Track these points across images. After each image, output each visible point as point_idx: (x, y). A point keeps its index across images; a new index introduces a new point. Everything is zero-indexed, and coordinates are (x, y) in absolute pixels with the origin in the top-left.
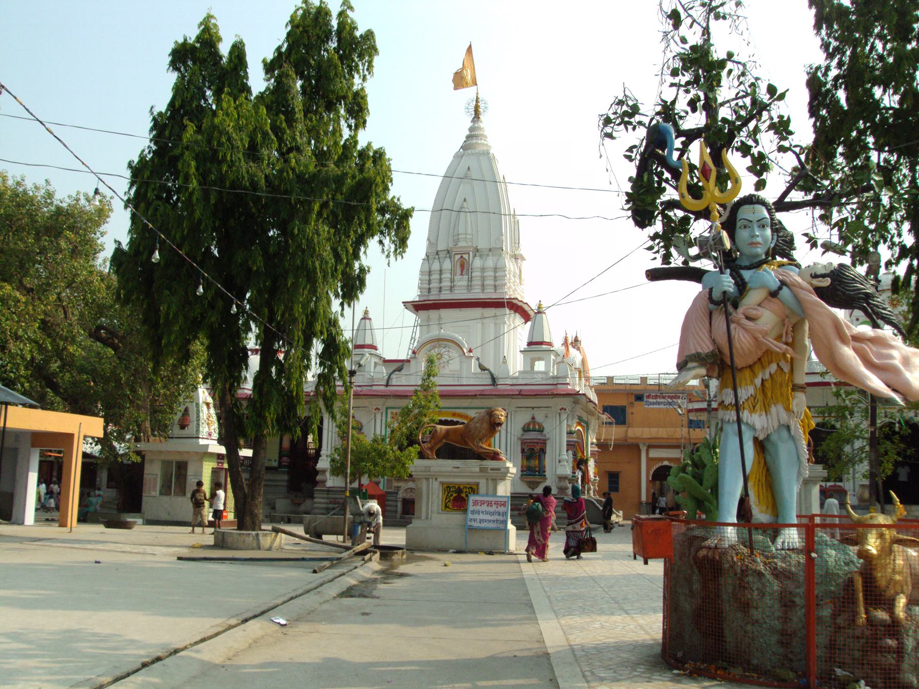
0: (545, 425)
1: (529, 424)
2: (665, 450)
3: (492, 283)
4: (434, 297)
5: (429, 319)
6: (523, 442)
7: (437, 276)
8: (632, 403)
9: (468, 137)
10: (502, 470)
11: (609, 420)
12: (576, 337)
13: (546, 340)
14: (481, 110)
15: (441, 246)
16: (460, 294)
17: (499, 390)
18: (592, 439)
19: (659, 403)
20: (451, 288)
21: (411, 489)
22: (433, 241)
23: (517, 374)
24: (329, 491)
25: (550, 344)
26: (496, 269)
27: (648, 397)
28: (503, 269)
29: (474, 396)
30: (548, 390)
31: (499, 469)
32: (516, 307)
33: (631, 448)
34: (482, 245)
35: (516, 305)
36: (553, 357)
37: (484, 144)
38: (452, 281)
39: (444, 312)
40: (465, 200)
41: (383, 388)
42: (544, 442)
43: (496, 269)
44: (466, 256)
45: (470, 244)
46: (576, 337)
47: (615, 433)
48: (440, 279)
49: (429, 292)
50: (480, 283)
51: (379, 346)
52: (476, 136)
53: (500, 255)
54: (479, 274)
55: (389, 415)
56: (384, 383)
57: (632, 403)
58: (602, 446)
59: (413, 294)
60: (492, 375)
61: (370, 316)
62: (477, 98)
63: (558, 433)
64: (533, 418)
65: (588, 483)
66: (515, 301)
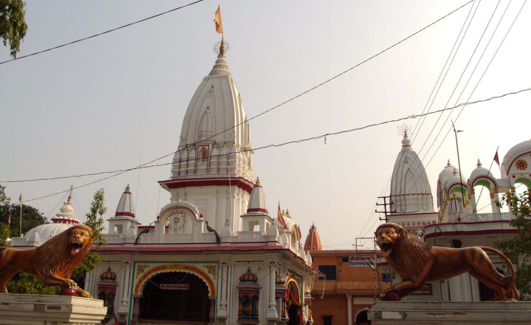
0: (258, 276)
1: (244, 276)
2: (363, 299)
3: (225, 166)
4: (183, 176)
5: (178, 195)
6: (241, 290)
7: (185, 163)
8: (340, 263)
9: (215, 67)
10: (63, 309)
11: (320, 275)
13: (261, 207)
14: (225, 49)
15: (190, 141)
16: (201, 175)
17: (221, 247)
19: (360, 264)
20: (195, 171)
22: (184, 137)
23: (236, 235)
25: (264, 211)
27: (352, 259)
31: (58, 308)
33: (339, 297)
34: (219, 139)
35: (243, 183)
36: (266, 221)
37: (225, 72)
38: (196, 166)
39: (189, 189)
40: (208, 108)
41: (132, 246)
42: (257, 290)
44: (206, 148)
47: (326, 286)
49: (179, 175)
51: (137, 215)
52: (220, 66)
53: (232, 147)
55: (136, 268)
56: (133, 241)
57: (340, 263)
58: (315, 294)
59: (167, 175)
61: (131, 191)
62: (222, 42)
64: (249, 270)
66: (242, 180)
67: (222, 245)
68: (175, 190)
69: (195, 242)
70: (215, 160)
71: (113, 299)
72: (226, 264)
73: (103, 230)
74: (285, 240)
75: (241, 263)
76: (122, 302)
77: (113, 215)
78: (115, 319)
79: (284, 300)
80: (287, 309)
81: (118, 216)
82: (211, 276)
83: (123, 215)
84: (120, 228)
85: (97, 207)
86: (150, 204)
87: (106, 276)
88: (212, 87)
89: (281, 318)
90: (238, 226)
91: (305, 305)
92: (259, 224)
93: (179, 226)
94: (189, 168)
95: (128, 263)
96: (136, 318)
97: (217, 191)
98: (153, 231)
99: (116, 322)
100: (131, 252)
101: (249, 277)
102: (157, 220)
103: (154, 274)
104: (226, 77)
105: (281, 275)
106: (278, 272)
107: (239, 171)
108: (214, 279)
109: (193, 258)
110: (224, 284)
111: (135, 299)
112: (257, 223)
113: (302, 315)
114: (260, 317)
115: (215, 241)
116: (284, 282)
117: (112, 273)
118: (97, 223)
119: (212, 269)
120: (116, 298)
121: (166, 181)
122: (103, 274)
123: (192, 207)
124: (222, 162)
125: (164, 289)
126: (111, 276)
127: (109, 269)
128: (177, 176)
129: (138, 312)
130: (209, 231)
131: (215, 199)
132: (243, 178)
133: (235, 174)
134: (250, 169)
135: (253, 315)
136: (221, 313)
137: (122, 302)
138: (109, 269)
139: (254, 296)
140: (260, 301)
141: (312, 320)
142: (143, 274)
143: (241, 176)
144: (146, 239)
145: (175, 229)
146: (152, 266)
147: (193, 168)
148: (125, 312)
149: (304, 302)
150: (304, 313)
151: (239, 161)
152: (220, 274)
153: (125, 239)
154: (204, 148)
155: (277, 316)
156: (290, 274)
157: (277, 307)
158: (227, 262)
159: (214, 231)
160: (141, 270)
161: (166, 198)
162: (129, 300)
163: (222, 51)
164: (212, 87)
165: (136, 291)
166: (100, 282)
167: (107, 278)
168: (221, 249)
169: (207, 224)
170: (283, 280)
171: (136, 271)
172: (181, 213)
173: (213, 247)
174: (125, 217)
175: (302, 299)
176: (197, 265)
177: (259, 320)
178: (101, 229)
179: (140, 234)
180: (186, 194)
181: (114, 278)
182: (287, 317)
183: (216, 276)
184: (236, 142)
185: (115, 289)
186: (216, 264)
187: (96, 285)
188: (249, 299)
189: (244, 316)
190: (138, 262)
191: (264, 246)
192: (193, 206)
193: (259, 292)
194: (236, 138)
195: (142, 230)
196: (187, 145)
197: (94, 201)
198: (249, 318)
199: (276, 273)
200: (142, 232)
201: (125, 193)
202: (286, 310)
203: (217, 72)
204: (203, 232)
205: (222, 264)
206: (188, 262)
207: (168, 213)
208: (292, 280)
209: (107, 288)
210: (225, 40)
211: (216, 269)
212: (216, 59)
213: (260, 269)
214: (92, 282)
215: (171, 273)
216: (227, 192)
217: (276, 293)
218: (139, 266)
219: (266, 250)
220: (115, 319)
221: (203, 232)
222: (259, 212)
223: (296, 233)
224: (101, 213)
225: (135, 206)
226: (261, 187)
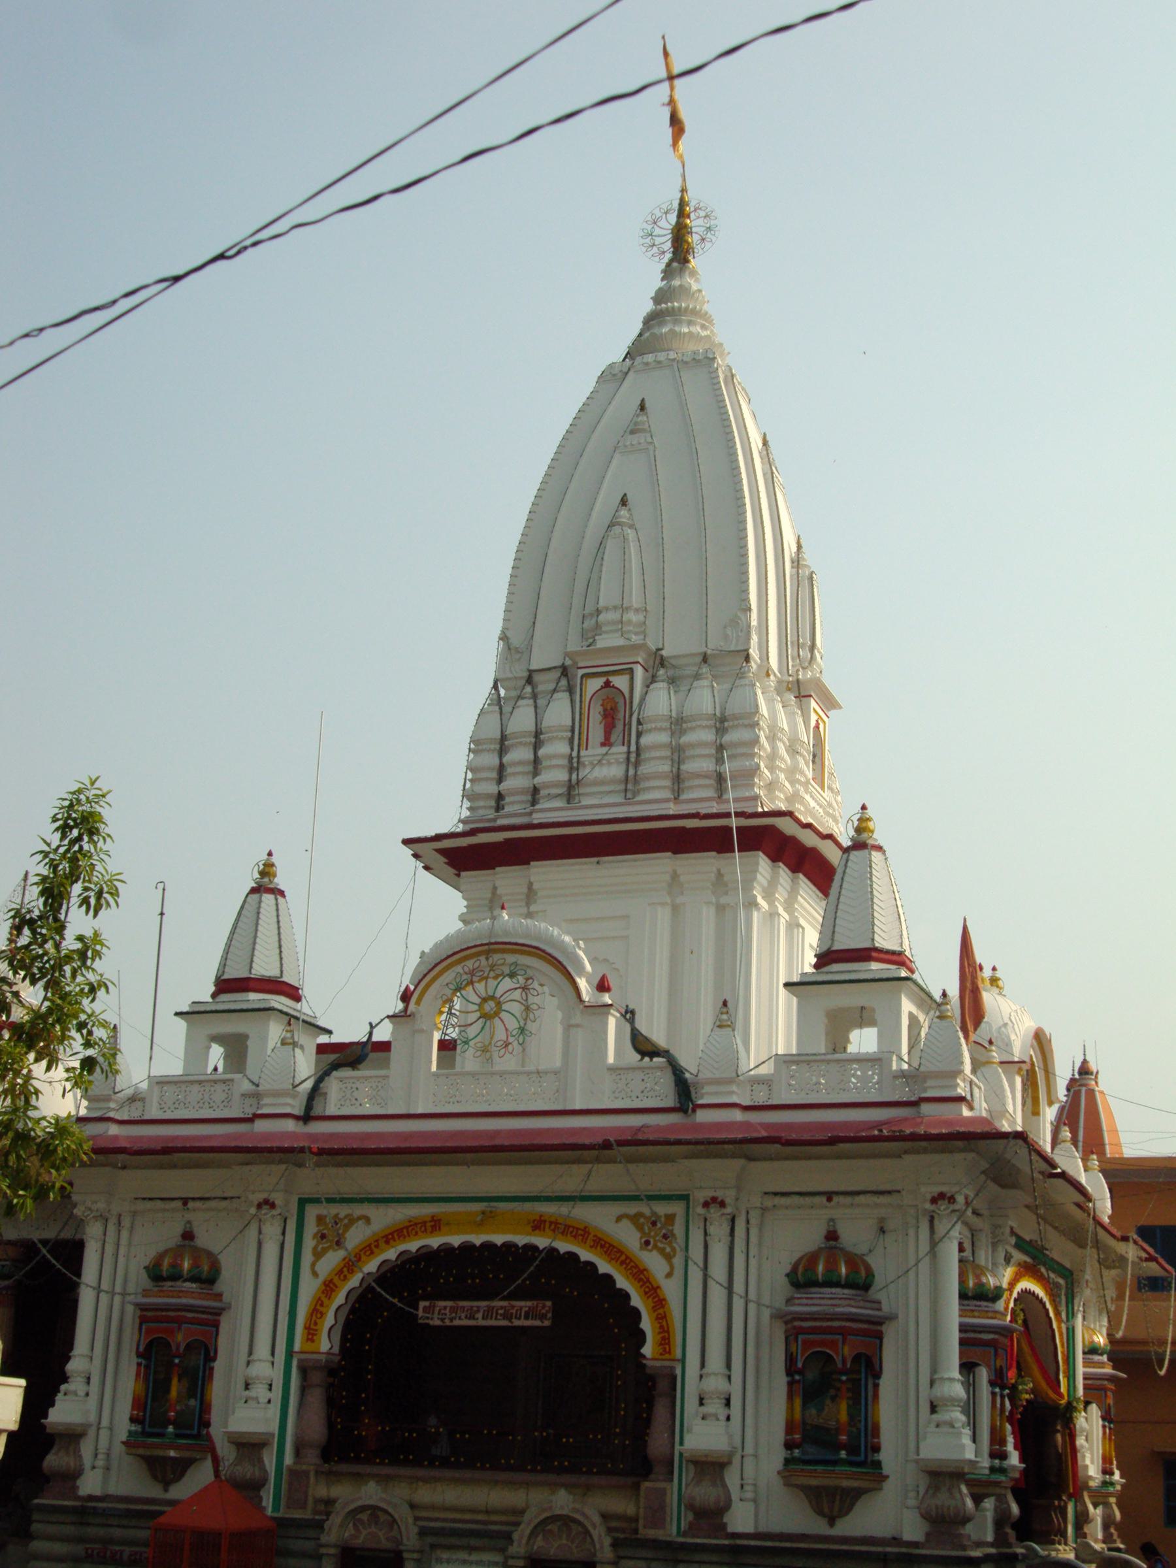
1: (811, 1259)
3: (708, 765)
4: (515, 810)
6: (795, 1329)
7: (526, 754)
9: (651, 320)
11: (1153, 1269)
12: (1085, 1062)
13: (884, 941)
14: (693, 239)
15: (545, 656)
16: (600, 804)
17: (702, 1126)
18: (1091, 1330)
20: (571, 791)
21: (374, 1510)
22: (516, 642)
24: (87, 1511)
25: (897, 958)
26: (722, 723)
28: (750, 719)
29: (602, 1149)
30: (879, 1125)
32: (802, 857)
34: (678, 643)
35: (793, 841)
36: (907, 1006)
37: (699, 338)
38: (574, 765)
39: (543, 873)
40: (624, 502)
41: (290, 1125)
42: (872, 1331)
43: (722, 723)
44: (620, 682)
45: (636, 639)
46: (1085, 1062)
48: (536, 761)
49: (498, 808)
50: (665, 767)
53: (741, 675)
54: (663, 738)
55: (311, 1228)
56: (298, 1108)
58: (1129, 1357)
59: (446, 814)
60: (677, 1072)
61: (280, 881)
62: (682, 204)
63: (927, 1302)
64: (832, 1236)
65: (1077, 1496)
66: (786, 826)
67: (702, 1116)
68: (475, 878)
69: (578, 1107)
70: (663, 738)
71: (209, 1374)
72: (722, 1204)
73: (101, 993)
74: (996, 1094)
75: (797, 1200)
76: (247, 1386)
77: (204, 991)
78: (216, 1461)
79: (998, 1380)
80: (1010, 1419)
81: (224, 997)
82: (654, 1263)
83: (246, 991)
84: (237, 1049)
85: (73, 877)
86: (368, 941)
87: (174, 1265)
88: (642, 407)
89: (985, 1463)
90: (773, 1029)
91: (1087, 1403)
92: (872, 1023)
93: (500, 1035)
94: (544, 778)
95: (273, 1206)
96: (312, 1457)
97: (675, 876)
98: (386, 1064)
99: (217, 1473)
100: (285, 1153)
101: (832, 1267)
102: (400, 1006)
103: (391, 1254)
104: (705, 362)
105: (983, 1258)
106: (967, 1245)
107: (771, 786)
108: (669, 1275)
109: (570, 1178)
110: (717, 1296)
111: (304, 1370)
112: (863, 1018)
113: (1074, 1450)
114: (887, 1456)
115: (670, 1102)
116: (995, 1295)
117: (199, 1254)
118: (68, 959)
119: (657, 1233)
120: (219, 1366)
121: (438, 838)
122: (161, 1257)
123: (562, 946)
124: (692, 746)
125: (437, 1323)
126: (196, 1264)
127: (188, 1235)
128: (491, 814)
129: (317, 1430)
130: (643, 1053)
131: (663, 916)
132: (790, 814)
133: (756, 798)
134: (819, 779)
135: (853, 1449)
136: (702, 1435)
137: (247, 1386)
138: (188, 1235)
139: (857, 1358)
140: (887, 1384)
141: (1117, 1476)
142: (341, 1254)
143: (783, 807)
144: (348, 1094)
145: (485, 1050)
146: (384, 1218)
147: (562, 776)
148: (259, 1428)
149: (1080, 1392)
150: (1080, 1441)
151: (772, 739)
152: (696, 1252)
153: (257, 1096)
154: (607, 684)
155: (970, 1454)
156: (1018, 1256)
157: (970, 1408)
158: (729, 1196)
159: (665, 1053)
160: (331, 1237)
161: (441, 910)
162: (277, 1375)
163: (681, 250)
164: (642, 407)
165: (311, 1333)
166: (146, 1293)
167: (175, 1277)
168: (700, 1136)
169: (631, 1021)
170: (991, 1281)
171: (309, 1243)
172: (512, 975)
173: (658, 1128)
174: (254, 998)
175: (1071, 1377)
176: (585, 1213)
177: (885, 1471)
178: (93, 990)
179: (327, 1073)
180: (530, 895)
181: (208, 1277)
182: (1014, 1459)
183: (678, 1261)
184: (754, 653)
185: (216, 1325)
186: (677, 1208)
187: (130, 1309)
188: (832, 1372)
189: (813, 1452)
190: (317, 1201)
191: (906, 1119)
192: (567, 939)
193: (879, 1336)
194: (755, 638)
195: (332, 1057)
196: (531, 672)
197: (55, 839)
198: (835, 1463)
199: (961, 1249)
200: (335, 1066)
201: (254, 891)
202: (1008, 1427)
203: (666, 351)
204: (611, 1060)
205: (706, 1205)
206: (548, 1199)
207: (449, 976)
208: (1026, 1284)
209: (180, 1321)
210: (692, 197)
211: (678, 1229)
212: (657, 283)
213: (882, 1230)
214: (113, 1293)
215: (467, 1248)
216: (720, 883)
217: (962, 1342)
218: (320, 1219)
219: (914, 1137)
220: (216, 1461)
221: (611, 1060)
222: (875, 966)
223: (1033, 1076)
224: (95, 903)
225: (300, 950)
226: (879, 848)
